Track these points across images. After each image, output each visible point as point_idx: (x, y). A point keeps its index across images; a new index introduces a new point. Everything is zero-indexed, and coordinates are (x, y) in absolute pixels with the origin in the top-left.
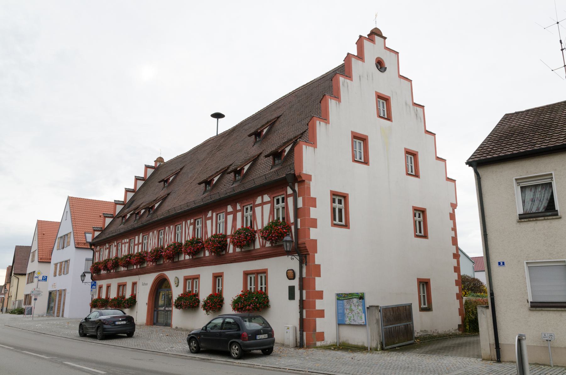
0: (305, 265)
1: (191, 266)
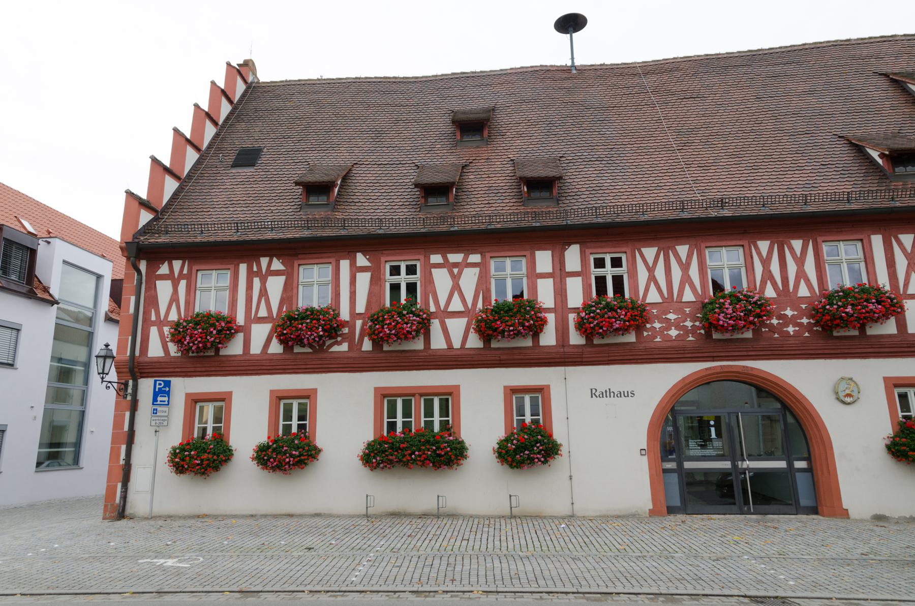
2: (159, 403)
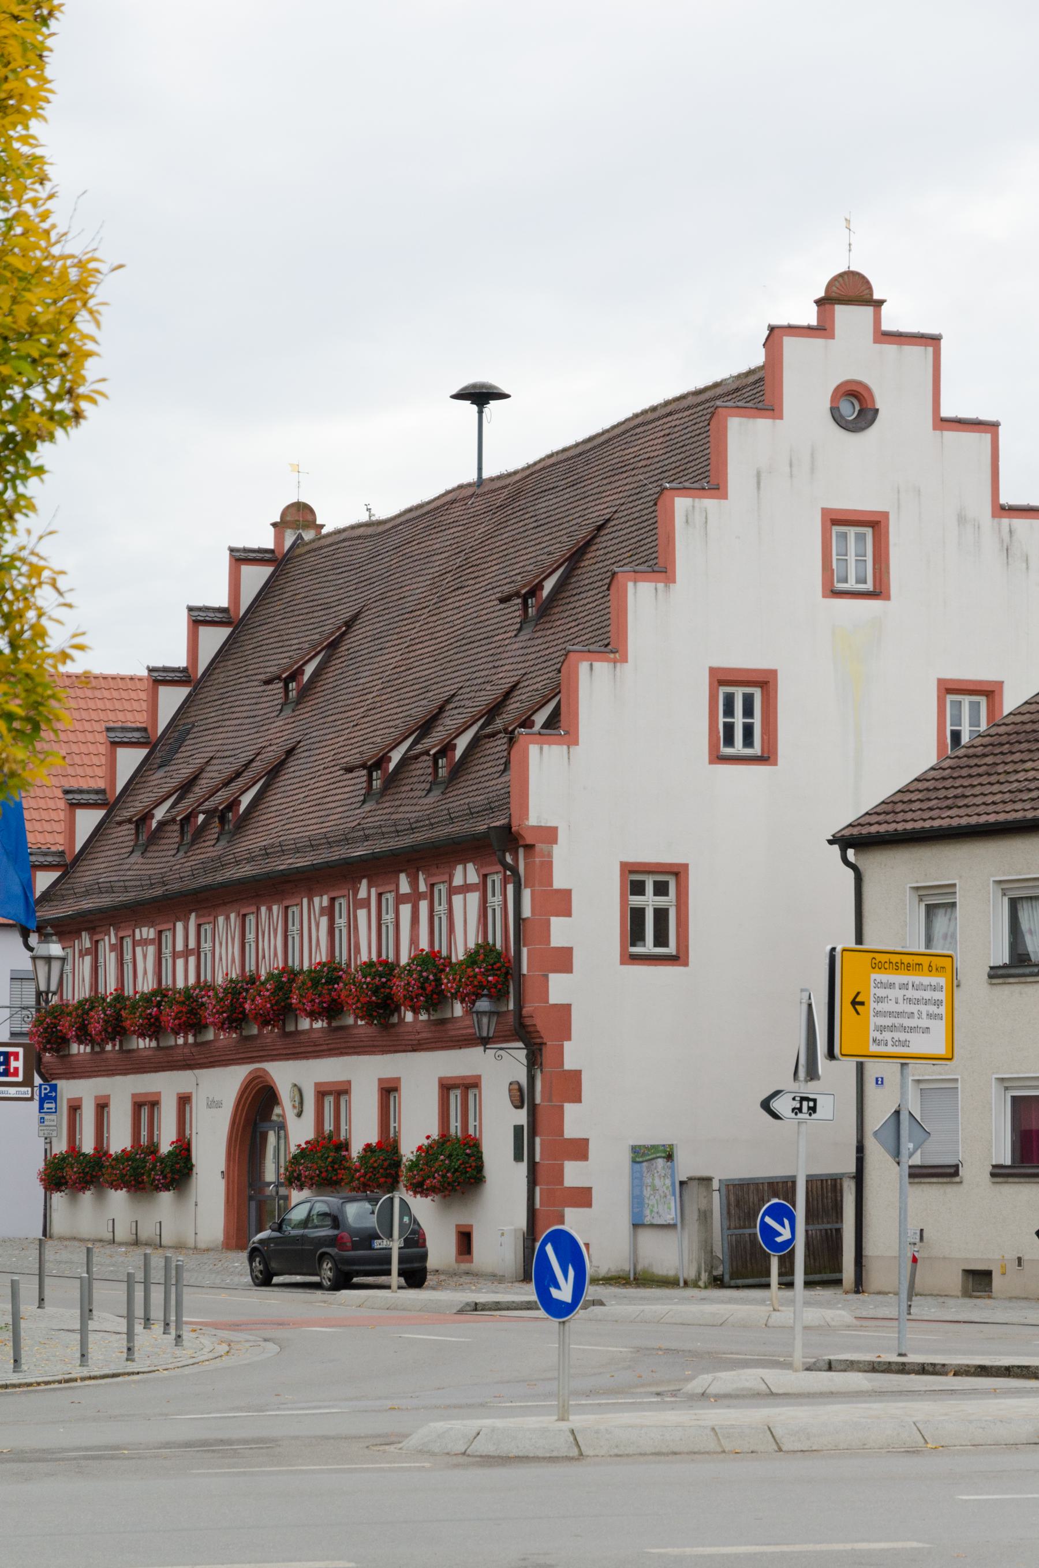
0: (539, 1071)
1: (330, 1050)
2: (45, 1110)
